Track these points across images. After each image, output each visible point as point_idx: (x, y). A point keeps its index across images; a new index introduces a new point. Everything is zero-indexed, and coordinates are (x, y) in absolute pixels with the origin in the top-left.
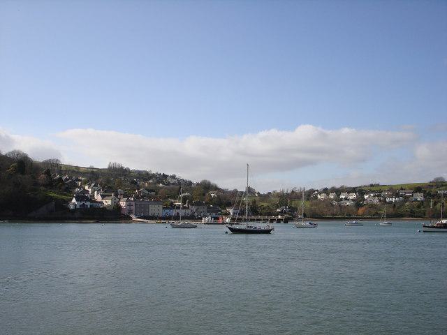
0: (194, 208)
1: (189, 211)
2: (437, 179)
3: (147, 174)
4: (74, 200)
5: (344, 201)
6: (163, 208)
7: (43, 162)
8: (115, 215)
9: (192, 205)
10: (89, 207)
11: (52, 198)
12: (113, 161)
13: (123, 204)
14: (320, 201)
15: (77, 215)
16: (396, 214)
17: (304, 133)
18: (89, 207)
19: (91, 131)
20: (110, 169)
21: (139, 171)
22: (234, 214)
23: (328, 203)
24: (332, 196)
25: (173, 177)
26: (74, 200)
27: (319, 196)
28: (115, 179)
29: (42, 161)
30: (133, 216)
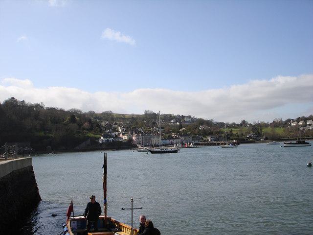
0: (183, 138)
1: (180, 140)
2: (91, 112)
3: (170, 116)
4: (102, 138)
5: (308, 126)
6: (162, 139)
7: (102, 113)
8: (129, 145)
9: (181, 136)
10: (111, 141)
11: (88, 138)
12: (147, 110)
13: (134, 138)
14: (292, 127)
15: (104, 147)
16: (277, 139)
17: (282, 81)
18: (111, 141)
19: (57, 87)
20: (146, 114)
21: (166, 115)
22: (211, 140)
23: (297, 128)
24: (301, 123)
25: (189, 117)
26: (102, 138)
27: (292, 124)
28: (134, 123)
29: (101, 112)
30: (139, 146)
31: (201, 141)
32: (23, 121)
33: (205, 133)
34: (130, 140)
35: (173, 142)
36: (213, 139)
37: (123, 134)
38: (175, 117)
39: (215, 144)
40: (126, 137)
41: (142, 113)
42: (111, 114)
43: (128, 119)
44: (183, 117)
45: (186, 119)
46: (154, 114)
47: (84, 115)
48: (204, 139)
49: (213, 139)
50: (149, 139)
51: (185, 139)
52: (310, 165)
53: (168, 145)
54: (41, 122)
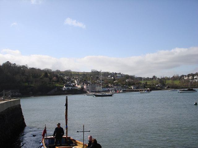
0: (116, 87)
1: (114, 88)
2: (57, 70)
3: (108, 73)
4: (64, 87)
5: (195, 80)
6: (102, 88)
7: (65, 71)
8: (82, 91)
9: (115, 86)
10: (70, 89)
11: (56, 87)
12: (93, 69)
13: (85, 87)
14: (185, 80)
15: (66, 92)
16: (175, 87)
17: (178, 51)
18: (70, 89)
19: (36, 55)
20: (92, 72)
21: (105, 72)
22: (134, 88)
23: (188, 81)
24: (190, 78)
25: (120, 74)
26: (64, 87)
27: (185, 78)
28: (85, 77)
29: (64, 70)
30: (88, 92)
31: (127, 89)
32: (15, 76)
33: (130, 84)
34: (82, 88)
35: (109, 89)
36: (135, 87)
37: (78, 84)
38: (111, 74)
39: (136, 91)
40: (79, 87)
41: (90, 71)
42: (70, 72)
43: (81, 75)
44: (116, 74)
45: (117, 75)
46: (98, 72)
47: (53, 72)
48: (129, 87)
49: (135, 87)
50: (95, 88)
51: (117, 88)
52: (196, 104)
53: (106, 91)
54: (26, 77)
